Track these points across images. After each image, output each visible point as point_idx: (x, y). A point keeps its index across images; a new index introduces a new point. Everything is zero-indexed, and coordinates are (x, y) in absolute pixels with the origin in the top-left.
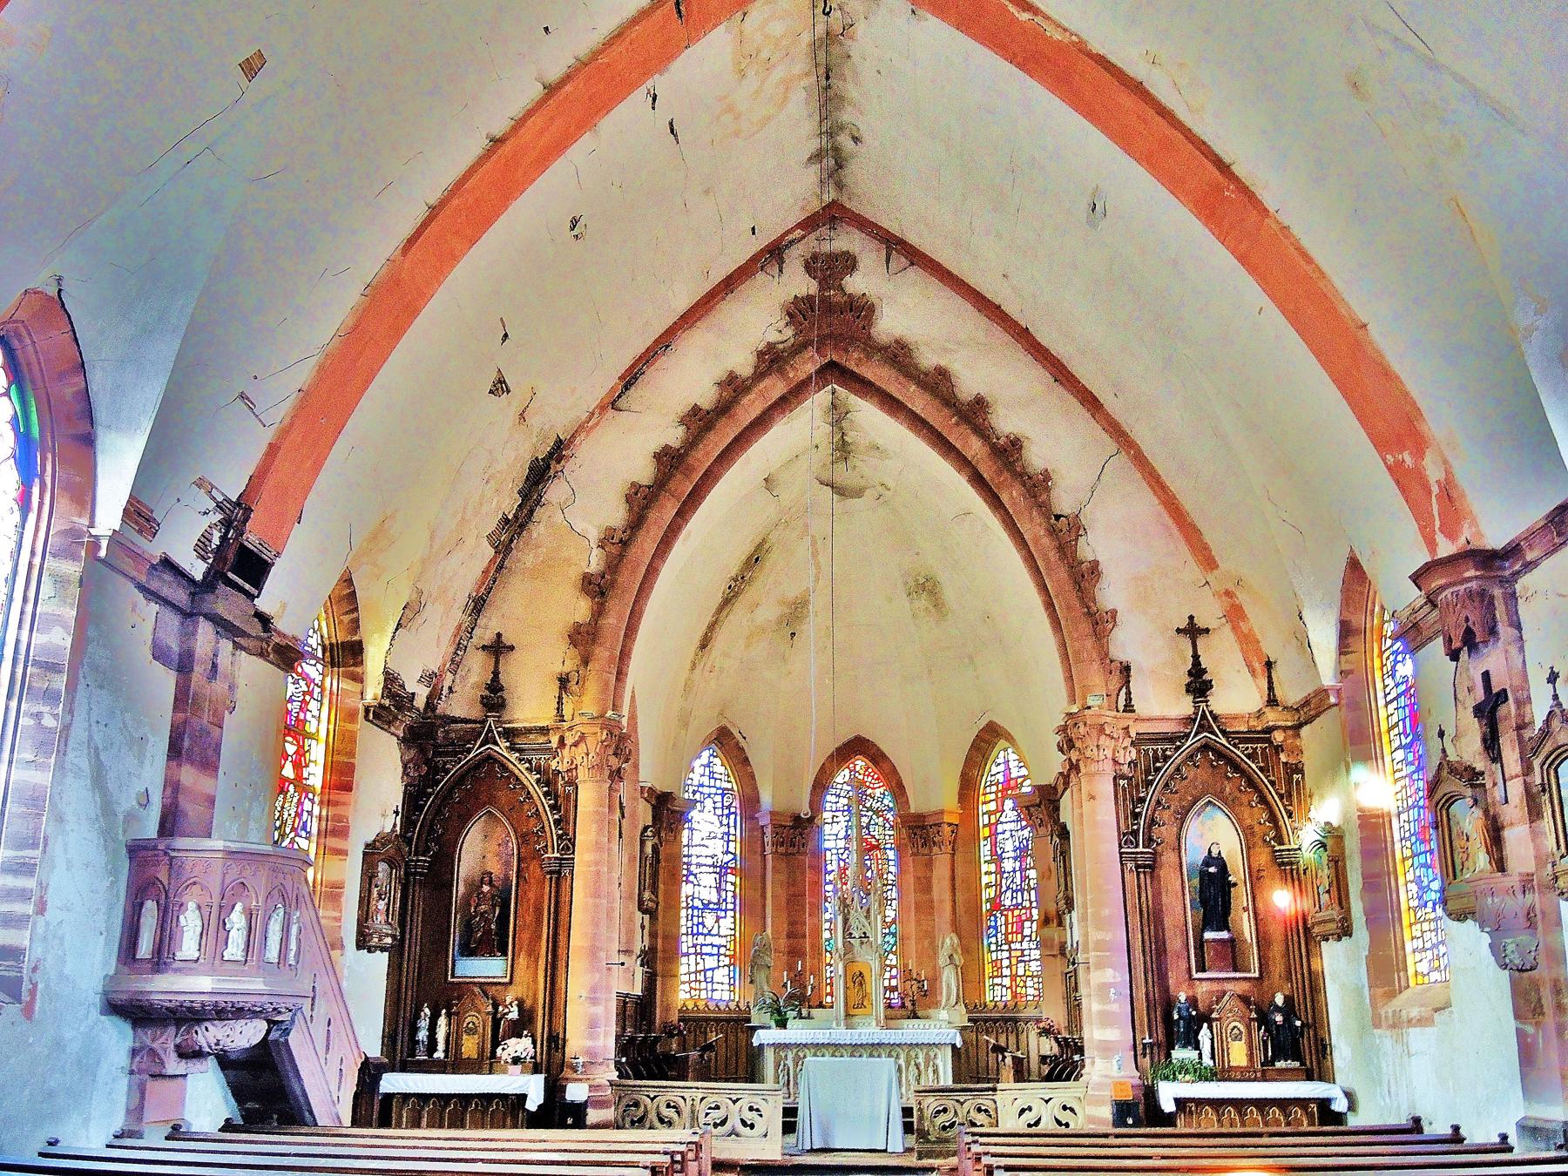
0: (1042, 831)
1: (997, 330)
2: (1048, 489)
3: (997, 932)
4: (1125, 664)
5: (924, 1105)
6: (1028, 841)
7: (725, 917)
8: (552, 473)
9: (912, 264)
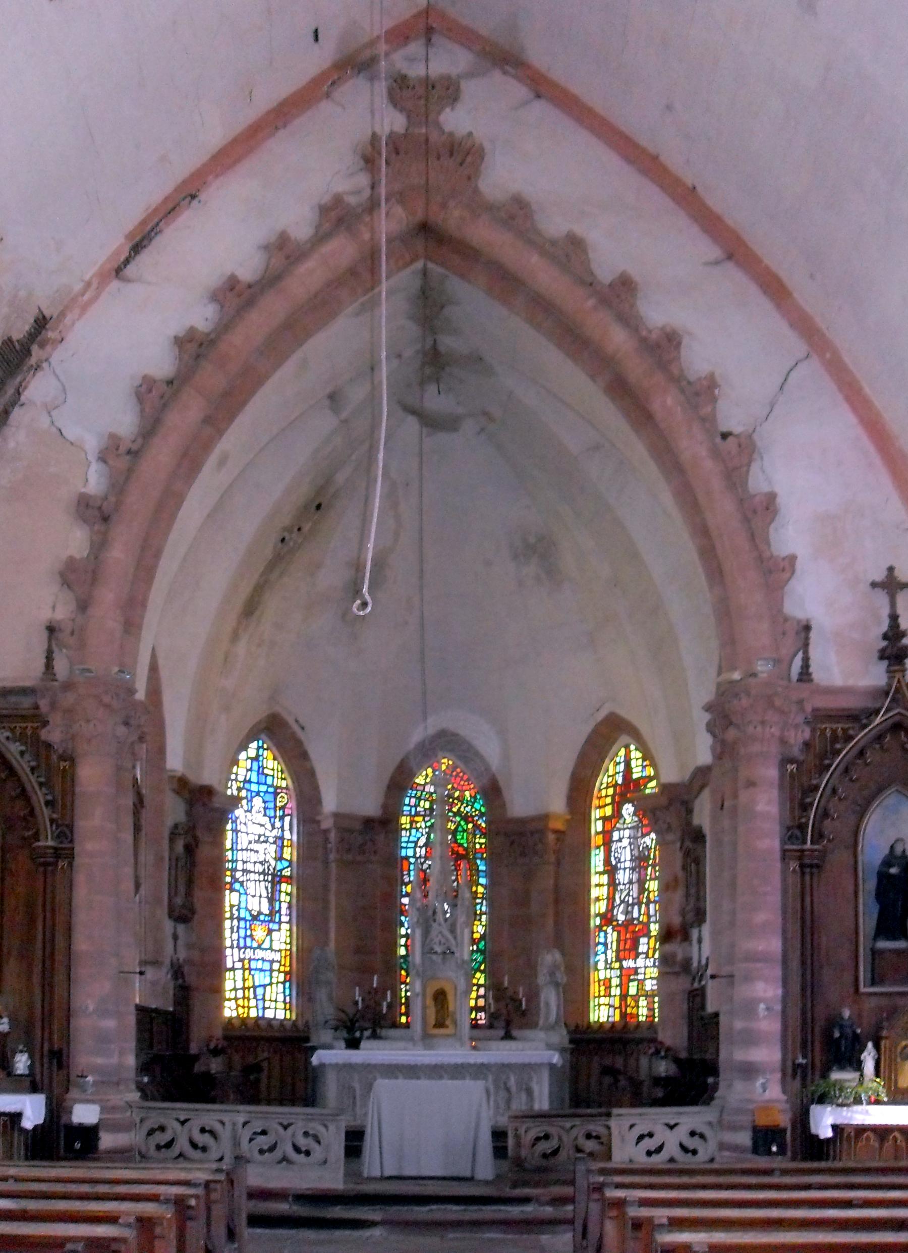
0: (670, 837)
1: (652, 191)
2: (714, 400)
3: (606, 948)
4: (804, 623)
5: (522, 1131)
6: (649, 849)
7: (279, 930)
8: (33, 361)
9: (538, 96)
